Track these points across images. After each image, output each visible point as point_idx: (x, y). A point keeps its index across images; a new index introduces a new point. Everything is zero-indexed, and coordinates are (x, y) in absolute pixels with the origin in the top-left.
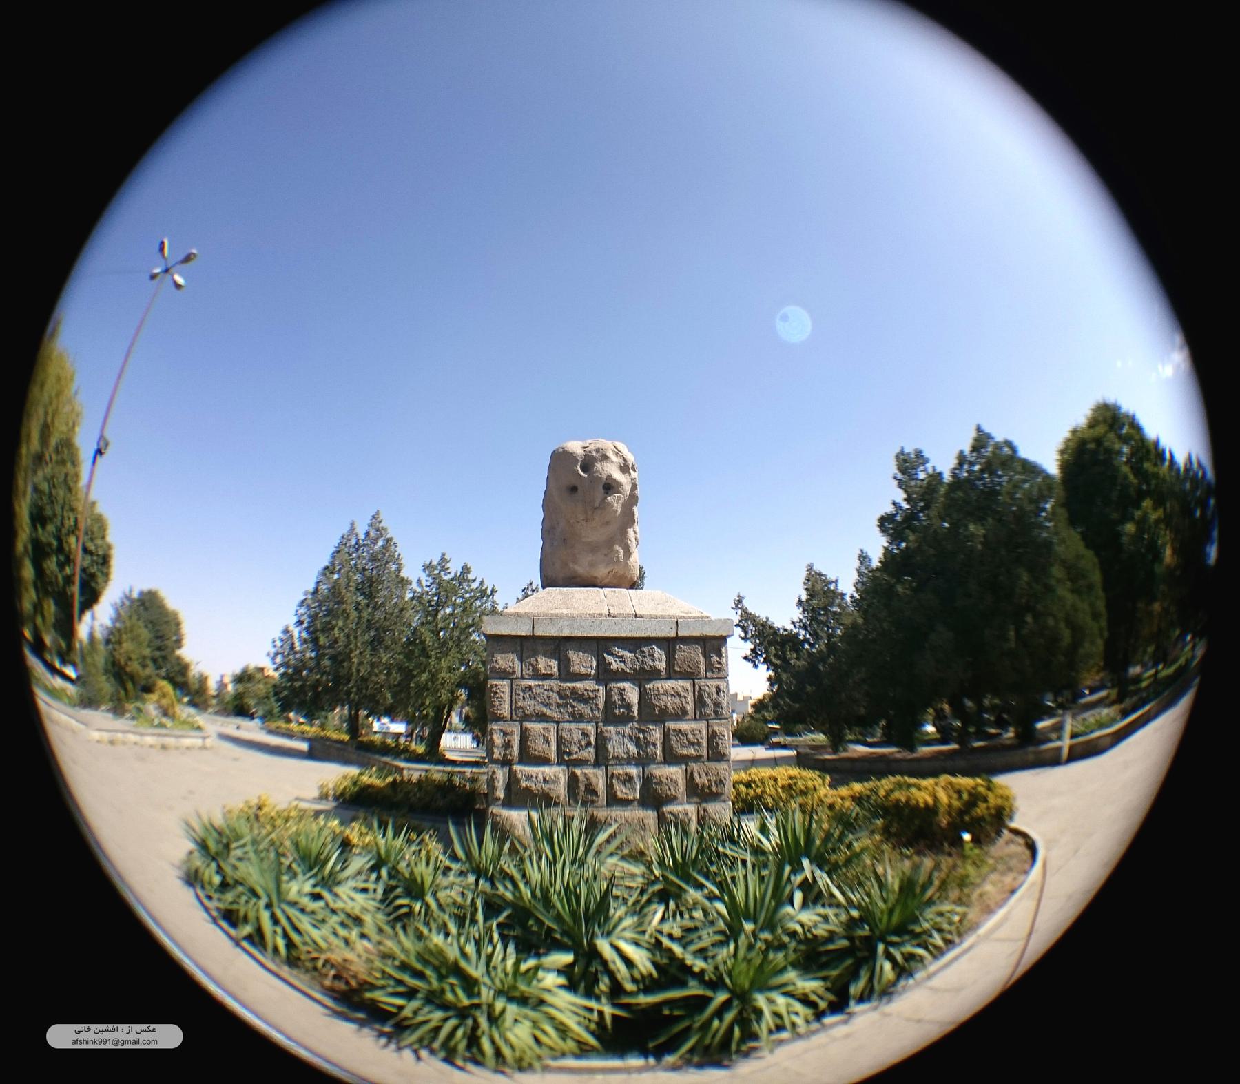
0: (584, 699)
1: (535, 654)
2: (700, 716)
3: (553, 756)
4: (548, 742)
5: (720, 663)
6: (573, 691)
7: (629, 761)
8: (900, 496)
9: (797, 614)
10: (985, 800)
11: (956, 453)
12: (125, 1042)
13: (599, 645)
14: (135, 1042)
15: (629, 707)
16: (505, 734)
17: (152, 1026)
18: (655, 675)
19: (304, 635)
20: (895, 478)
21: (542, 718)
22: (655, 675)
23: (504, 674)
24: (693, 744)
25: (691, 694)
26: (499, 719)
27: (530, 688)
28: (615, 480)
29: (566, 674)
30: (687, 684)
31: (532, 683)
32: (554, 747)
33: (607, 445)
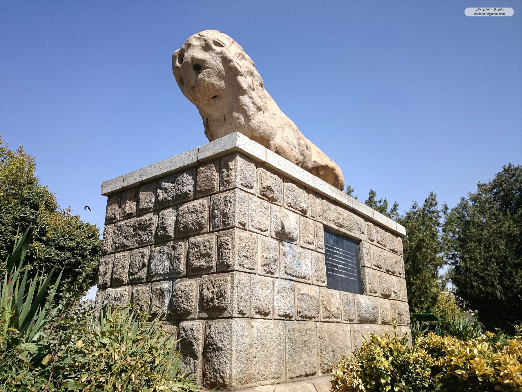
3: (125, 279)
5: (228, 176)
12: (493, 14)
14: (497, 14)
17: (503, 8)
24: (203, 255)
32: (127, 271)
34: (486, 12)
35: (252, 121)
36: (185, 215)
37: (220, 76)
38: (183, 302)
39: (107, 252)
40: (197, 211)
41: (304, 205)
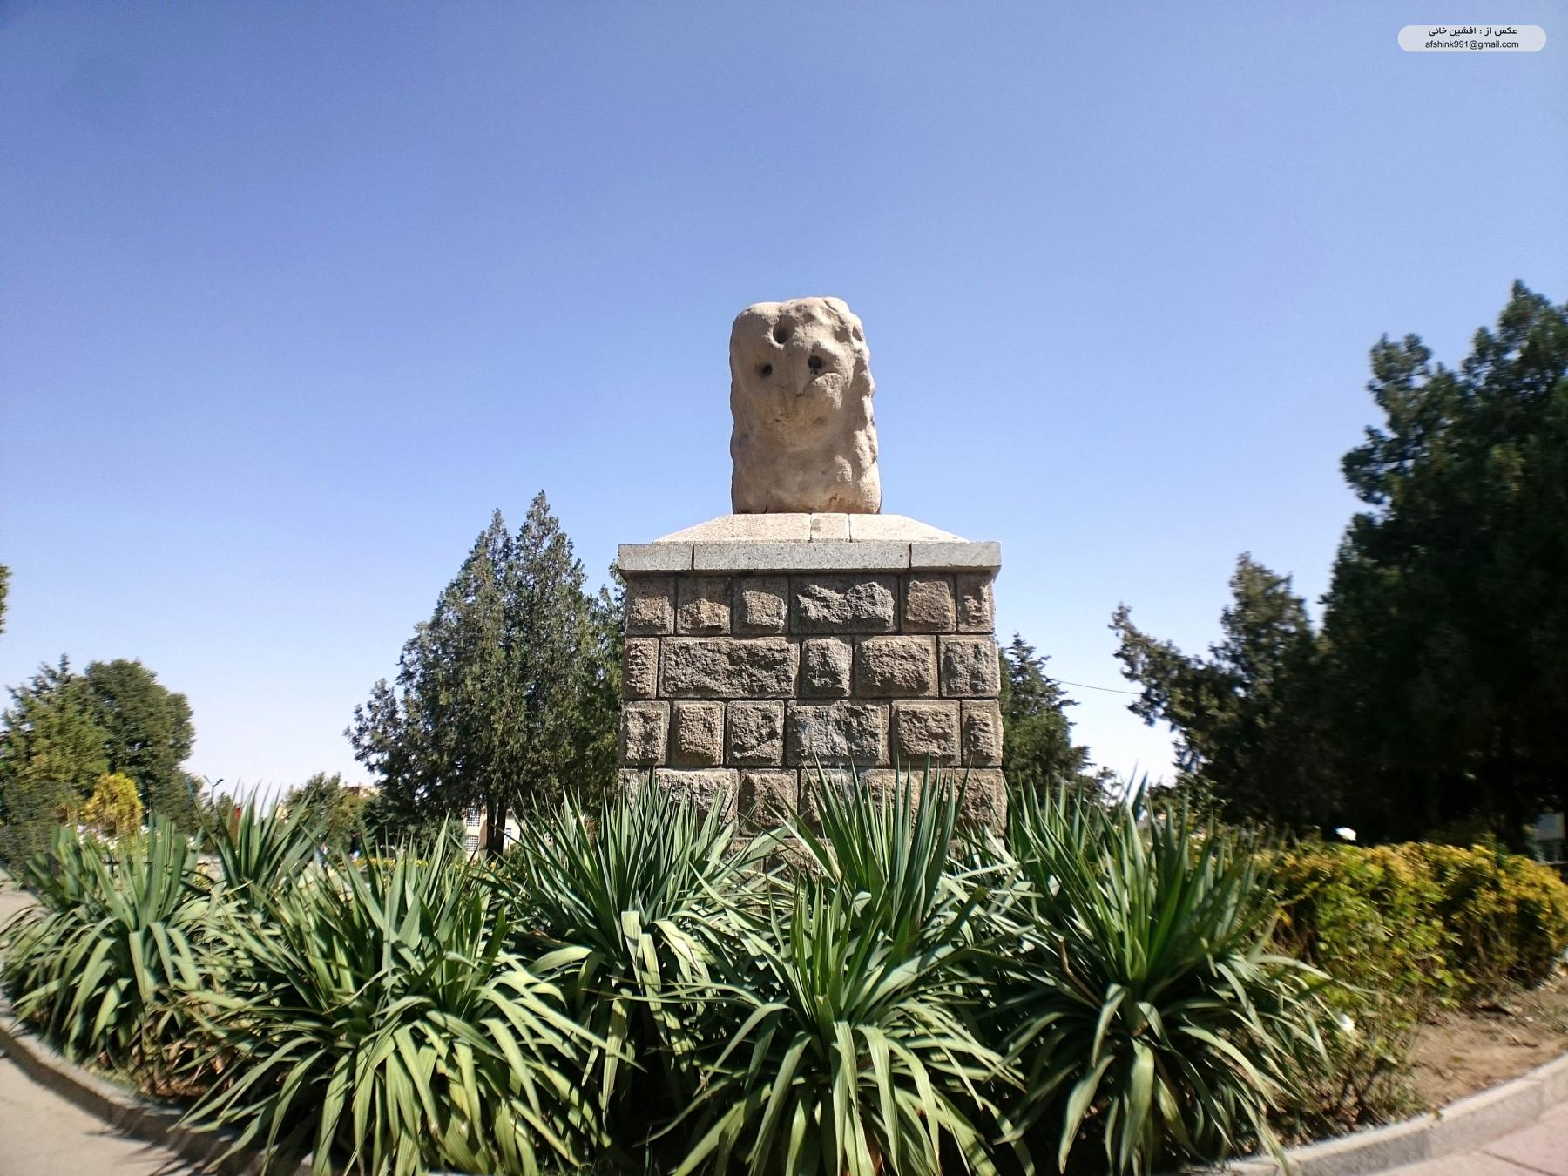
0: (768, 663)
1: (695, 597)
2: (953, 695)
3: (718, 753)
4: (710, 730)
5: (979, 610)
6: (751, 653)
7: (833, 761)
8: (1379, 419)
9: (1220, 635)
10: (1495, 886)
11: (1472, 332)
12: (1482, 45)
13: (791, 582)
14: (1495, 45)
15: (834, 675)
16: (647, 719)
18: (875, 626)
19: (414, 695)
20: (1371, 388)
21: (705, 694)
22: (875, 626)
23: (649, 629)
24: (936, 736)
25: (933, 657)
26: (637, 696)
27: (687, 648)
28: (825, 351)
29: (743, 626)
30: (927, 642)
31: (690, 641)
32: (720, 739)
33: (816, 304)
34: (1463, 38)
36: (885, 659)
40: (913, 658)
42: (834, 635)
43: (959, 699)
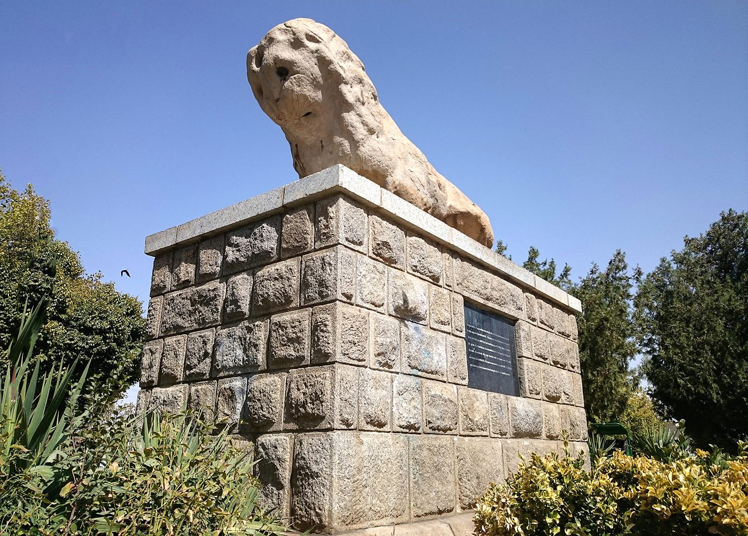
5: (327, 227)
24: (291, 340)
25: (297, 275)
28: (284, 61)
35: (361, 148)
37: (315, 85)
38: (262, 408)
39: (153, 335)
41: (436, 269)
42: (244, 271)
43: (163, 295)
